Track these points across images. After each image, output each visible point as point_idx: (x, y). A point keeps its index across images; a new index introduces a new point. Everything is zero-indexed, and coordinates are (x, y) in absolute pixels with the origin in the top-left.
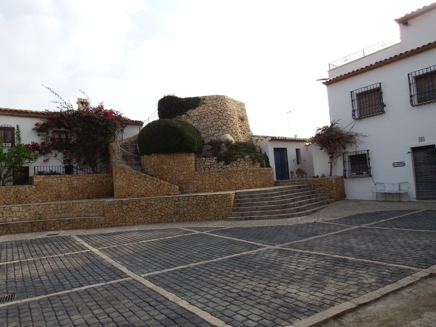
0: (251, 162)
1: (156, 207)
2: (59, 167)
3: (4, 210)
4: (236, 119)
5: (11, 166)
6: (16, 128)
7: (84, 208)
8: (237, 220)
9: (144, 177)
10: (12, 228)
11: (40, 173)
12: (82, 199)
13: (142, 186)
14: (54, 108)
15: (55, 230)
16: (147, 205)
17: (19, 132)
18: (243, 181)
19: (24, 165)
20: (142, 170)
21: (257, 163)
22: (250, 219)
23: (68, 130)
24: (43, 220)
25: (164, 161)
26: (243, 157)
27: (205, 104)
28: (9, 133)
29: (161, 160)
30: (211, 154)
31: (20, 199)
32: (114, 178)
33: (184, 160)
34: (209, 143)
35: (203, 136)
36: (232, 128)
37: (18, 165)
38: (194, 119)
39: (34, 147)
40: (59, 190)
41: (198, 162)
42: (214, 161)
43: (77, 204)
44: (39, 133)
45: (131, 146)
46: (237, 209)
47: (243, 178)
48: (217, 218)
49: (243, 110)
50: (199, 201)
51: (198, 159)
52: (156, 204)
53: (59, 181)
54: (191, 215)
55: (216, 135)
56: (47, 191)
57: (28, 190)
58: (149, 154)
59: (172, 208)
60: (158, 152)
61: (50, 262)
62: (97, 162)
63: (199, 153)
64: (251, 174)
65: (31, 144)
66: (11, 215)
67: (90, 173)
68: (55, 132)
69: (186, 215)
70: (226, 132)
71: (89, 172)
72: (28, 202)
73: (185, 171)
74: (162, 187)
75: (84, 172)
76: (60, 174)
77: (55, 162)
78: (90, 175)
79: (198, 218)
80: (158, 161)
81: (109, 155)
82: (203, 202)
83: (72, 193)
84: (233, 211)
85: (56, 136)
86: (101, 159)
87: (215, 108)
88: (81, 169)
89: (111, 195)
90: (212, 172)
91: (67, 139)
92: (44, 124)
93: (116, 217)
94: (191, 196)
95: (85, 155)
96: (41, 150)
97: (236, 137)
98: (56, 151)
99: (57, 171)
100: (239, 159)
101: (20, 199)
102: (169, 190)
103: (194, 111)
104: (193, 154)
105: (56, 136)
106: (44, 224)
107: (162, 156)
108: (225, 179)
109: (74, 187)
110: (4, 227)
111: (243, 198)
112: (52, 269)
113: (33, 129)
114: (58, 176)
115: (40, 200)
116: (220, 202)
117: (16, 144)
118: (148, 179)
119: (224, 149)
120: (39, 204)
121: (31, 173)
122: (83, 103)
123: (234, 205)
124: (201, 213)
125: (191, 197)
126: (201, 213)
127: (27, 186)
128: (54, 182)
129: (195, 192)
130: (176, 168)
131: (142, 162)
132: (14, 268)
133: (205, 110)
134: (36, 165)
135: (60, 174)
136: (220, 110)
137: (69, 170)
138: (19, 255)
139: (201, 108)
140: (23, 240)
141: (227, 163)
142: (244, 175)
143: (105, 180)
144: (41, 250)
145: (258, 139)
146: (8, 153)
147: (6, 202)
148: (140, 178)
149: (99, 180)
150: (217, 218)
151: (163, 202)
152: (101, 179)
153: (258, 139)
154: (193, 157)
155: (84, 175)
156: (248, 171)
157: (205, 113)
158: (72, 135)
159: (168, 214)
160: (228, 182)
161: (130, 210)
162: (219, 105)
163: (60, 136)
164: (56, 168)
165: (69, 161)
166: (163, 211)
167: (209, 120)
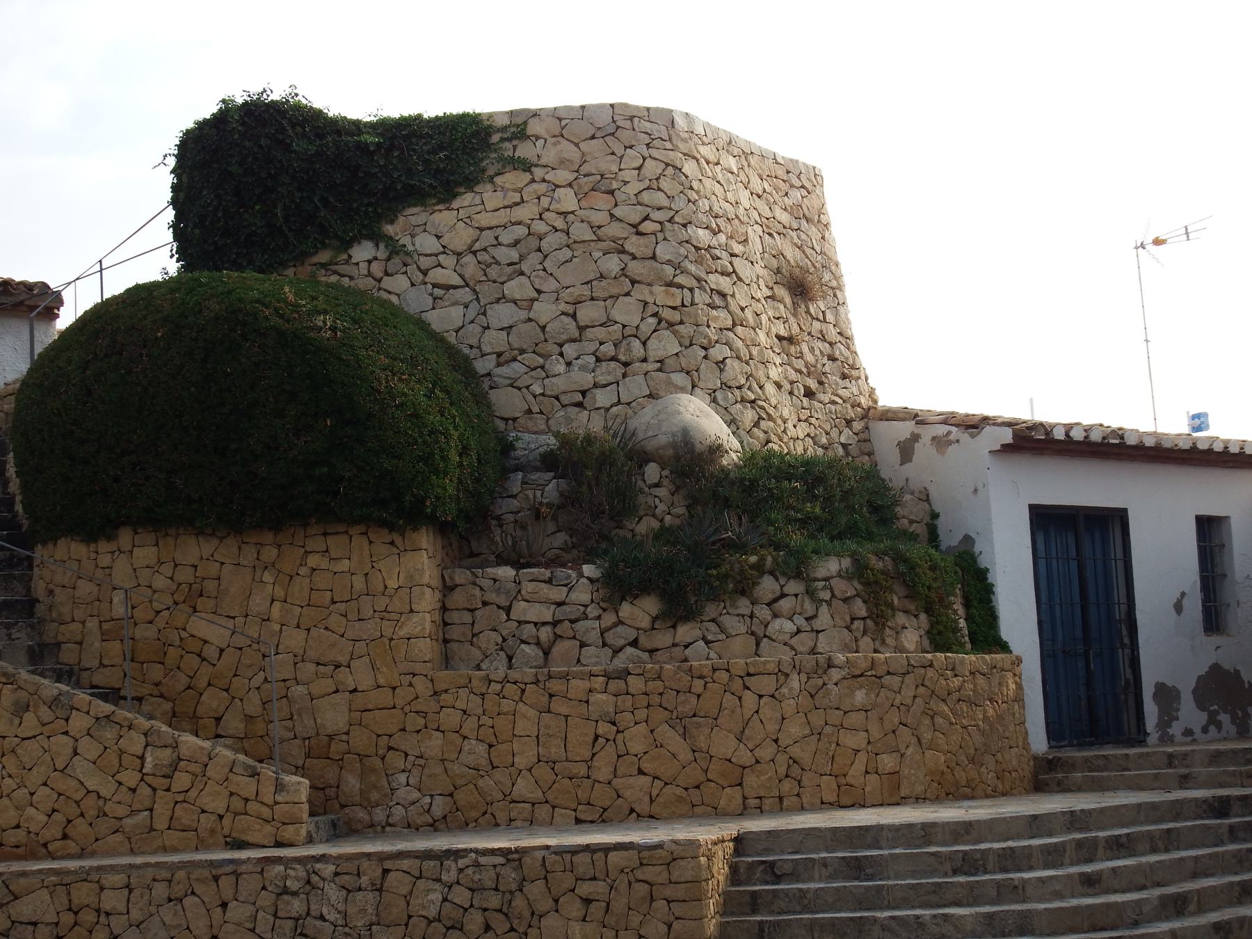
0: (860, 608)
4: (752, 287)
9: (54, 703)
13: (35, 777)
16: (68, 918)
18: (795, 751)
21: (901, 619)
25: (210, 586)
26: (796, 567)
29: (185, 575)
30: (561, 538)
34: (549, 462)
35: (506, 402)
36: (718, 352)
38: (437, 275)
41: (458, 598)
42: (582, 594)
47: (795, 729)
49: (810, 217)
50: (461, 896)
51: (461, 576)
52: (136, 915)
55: (603, 398)
58: (96, 529)
60: (164, 516)
63: (469, 533)
64: (860, 696)
70: (679, 379)
74: (182, 780)
80: (160, 582)
82: (494, 901)
87: (603, 202)
90: (565, 677)
94: (400, 855)
97: (749, 416)
100: (768, 586)
102: (237, 804)
103: (443, 218)
107: (192, 550)
111: (793, 876)
116: (619, 904)
118: (79, 722)
119: (661, 505)
123: (723, 926)
125: (406, 864)
130: (294, 639)
133: (523, 213)
136: (634, 215)
139: (492, 198)
141: (678, 610)
142: (805, 700)
145: (915, 438)
151: (189, 901)
153: (915, 438)
156: (835, 674)
157: (521, 231)
160: (685, 755)
167: (550, 285)
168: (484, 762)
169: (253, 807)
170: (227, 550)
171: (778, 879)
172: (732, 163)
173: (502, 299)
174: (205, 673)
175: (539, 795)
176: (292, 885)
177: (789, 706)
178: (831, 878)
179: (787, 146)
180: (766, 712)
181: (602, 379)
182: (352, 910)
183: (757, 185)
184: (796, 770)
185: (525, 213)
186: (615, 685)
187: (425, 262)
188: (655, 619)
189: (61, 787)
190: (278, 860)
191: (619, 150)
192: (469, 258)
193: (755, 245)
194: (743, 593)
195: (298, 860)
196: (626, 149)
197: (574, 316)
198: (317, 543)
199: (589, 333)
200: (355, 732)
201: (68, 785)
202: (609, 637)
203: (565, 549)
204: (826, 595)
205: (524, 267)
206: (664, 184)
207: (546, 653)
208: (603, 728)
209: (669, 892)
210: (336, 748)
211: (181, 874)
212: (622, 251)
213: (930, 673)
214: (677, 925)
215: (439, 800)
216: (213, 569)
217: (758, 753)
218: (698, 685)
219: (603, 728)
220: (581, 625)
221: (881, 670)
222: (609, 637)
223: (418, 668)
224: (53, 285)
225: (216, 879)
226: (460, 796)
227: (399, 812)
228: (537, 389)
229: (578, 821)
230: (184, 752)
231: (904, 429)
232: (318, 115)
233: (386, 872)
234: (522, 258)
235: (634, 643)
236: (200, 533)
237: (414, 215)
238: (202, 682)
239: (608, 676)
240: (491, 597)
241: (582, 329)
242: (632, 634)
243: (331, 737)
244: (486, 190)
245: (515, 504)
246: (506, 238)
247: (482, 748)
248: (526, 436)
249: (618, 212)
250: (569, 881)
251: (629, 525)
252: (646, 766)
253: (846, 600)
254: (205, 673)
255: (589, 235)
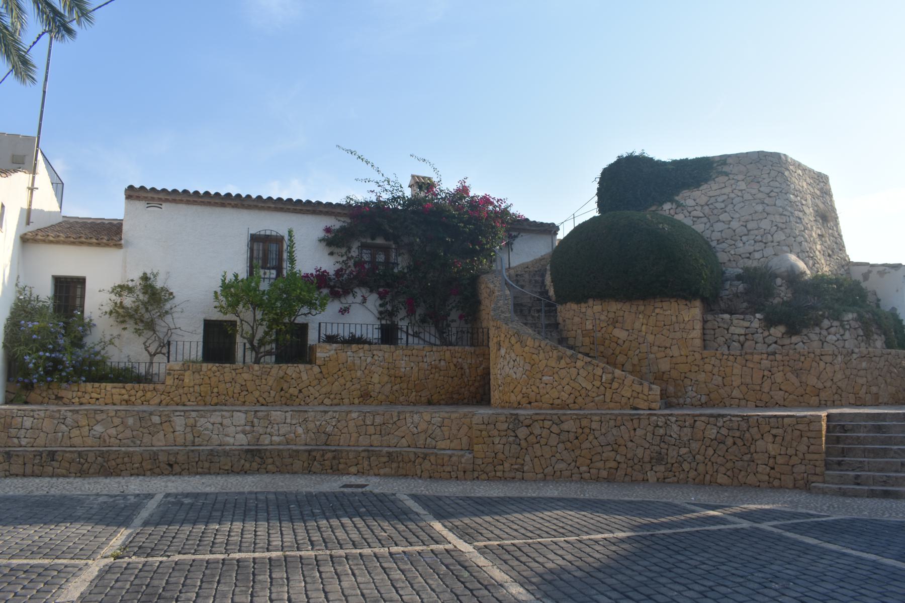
0: (861, 332)
1: (602, 438)
2: (370, 327)
3: (255, 417)
5: (274, 319)
6: (286, 238)
7: (423, 426)
8: (844, 494)
10: (270, 460)
11: (331, 339)
12: (414, 404)
13: (564, 382)
14: (362, 194)
15: (358, 473)
16: (580, 431)
17: (292, 245)
18: (839, 384)
19: (300, 320)
20: (562, 341)
21: (876, 337)
22: (886, 494)
23: (391, 243)
24: (333, 448)
25: (620, 319)
26: (837, 317)
27: (727, 174)
28: (274, 247)
29: (611, 315)
30: (745, 305)
31: (288, 395)
32: (492, 356)
33: (674, 318)
34: (739, 277)
36: (799, 239)
37: (286, 320)
38: (694, 213)
39: (321, 279)
40: (368, 379)
41: (709, 325)
42: (756, 324)
43: (408, 415)
44: (333, 249)
45: (530, 281)
46: (839, 463)
47: (839, 376)
48: (776, 483)
49: (826, 193)
50: (724, 431)
51: (709, 317)
52: (603, 431)
53: (369, 360)
54: (701, 468)
55: (757, 255)
56: (342, 381)
57: (304, 376)
58: (580, 299)
59: (647, 445)
60: (603, 296)
61: (356, 572)
62: (449, 318)
63: (711, 303)
64: (864, 365)
65: (314, 273)
66: (268, 430)
67: (435, 345)
68: (363, 246)
69: (686, 466)
70: (785, 248)
71: (433, 340)
72: (302, 403)
73: (675, 348)
74: (615, 385)
75: (421, 342)
76: (370, 343)
77: (362, 315)
78: (435, 348)
79: (721, 479)
80: (603, 317)
81: (479, 303)
82: (737, 434)
83: (395, 388)
84: (828, 466)
85: (366, 257)
86: (460, 312)
87: (756, 186)
88: (416, 335)
89: (482, 397)
90: (752, 354)
91: (387, 262)
92: (342, 229)
93: (500, 456)
94: (701, 415)
95: (425, 302)
96: (335, 286)
97: (811, 262)
98: (364, 290)
99: (365, 336)
100: (826, 323)
101: (288, 395)
102: (635, 394)
103: (696, 193)
104: (698, 303)
105: (366, 257)
106: (334, 458)
107: (614, 306)
108: (789, 375)
109: (401, 374)
110: (253, 456)
111: (852, 430)
112: (363, 595)
113: (320, 241)
114: (366, 346)
115: (327, 401)
116: (788, 438)
117: (285, 272)
118: (580, 364)
119: (783, 293)
120: (326, 409)
121: (312, 337)
122: (423, 184)
123: (827, 448)
124: (729, 465)
125: (703, 418)
126: (729, 465)
127: (302, 367)
128: (357, 362)
129: (702, 406)
130: (650, 338)
131: (560, 320)
132: (270, 577)
133: (725, 191)
134: (323, 320)
135: (370, 343)
136: (767, 190)
137: (388, 335)
138: (282, 534)
139: (715, 186)
140: (291, 493)
141: (792, 331)
143: (469, 361)
144: (331, 527)
145: (870, 272)
146: (269, 292)
147: (261, 399)
148: (560, 358)
149: (455, 360)
150: (776, 483)
151: (622, 427)
152: (460, 360)
153: (870, 272)
154: (694, 312)
155: (421, 347)
156: (855, 356)
157: (725, 197)
158: (398, 254)
159: (636, 461)
160: (797, 384)
161: (535, 440)
162: (765, 176)
163: (373, 257)
164: (364, 327)
165: (391, 314)
166: (622, 449)
167: (737, 215)
168: (721, 383)
169: (640, 396)
170: (626, 306)
171: (846, 431)
172: (800, 172)
173: (719, 221)
174: (618, 349)
175: (742, 396)
176: (660, 424)
177: (837, 367)
178: (869, 431)
179: (817, 168)
180: (828, 369)
181: (757, 249)
182: (682, 434)
183: (808, 180)
184: (839, 391)
185: (727, 191)
186: (771, 357)
187: (690, 209)
188: (783, 334)
189: (573, 385)
190: (655, 415)
191: (761, 167)
192: (706, 207)
193: (810, 202)
194: (817, 325)
195: (662, 415)
196: (767, 167)
197: (746, 226)
198: (659, 305)
199: (752, 232)
200: (673, 371)
201: (576, 385)
202: (766, 340)
203: (747, 309)
204: (848, 327)
205: (727, 209)
206: (778, 179)
207: (742, 346)
208: (766, 373)
209: (809, 434)
210: (666, 377)
211: (619, 418)
212: (763, 203)
213: (890, 356)
214: (812, 447)
215: (703, 397)
216: (621, 313)
217: (825, 384)
218: (802, 358)
219: (766, 373)
220: (756, 335)
221: (872, 355)
222: (766, 340)
223: (697, 349)
224: (557, 224)
225: (632, 420)
226: (712, 396)
227: (688, 400)
228: (732, 252)
229: (756, 406)
230: (616, 375)
231: (865, 269)
232: (651, 160)
233: (695, 421)
234: (726, 206)
235: (776, 343)
236: (617, 300)
237: (685, 193)
238: (617, 352)
239: (768, 354)
240: (721, 325)
241: (749, 231)
242: (775, 339)
243: (664, 373)
244: (711, 183)
245: (727, 292)
246: (720, 199)
247: (720, 379)
248: (730, 269)
249: (761, 189)
250: (767, 428)
251: (771, 300)
252: (782, 388)
253: (855, 329)
254: (618, 349)
255: (751, 198)
